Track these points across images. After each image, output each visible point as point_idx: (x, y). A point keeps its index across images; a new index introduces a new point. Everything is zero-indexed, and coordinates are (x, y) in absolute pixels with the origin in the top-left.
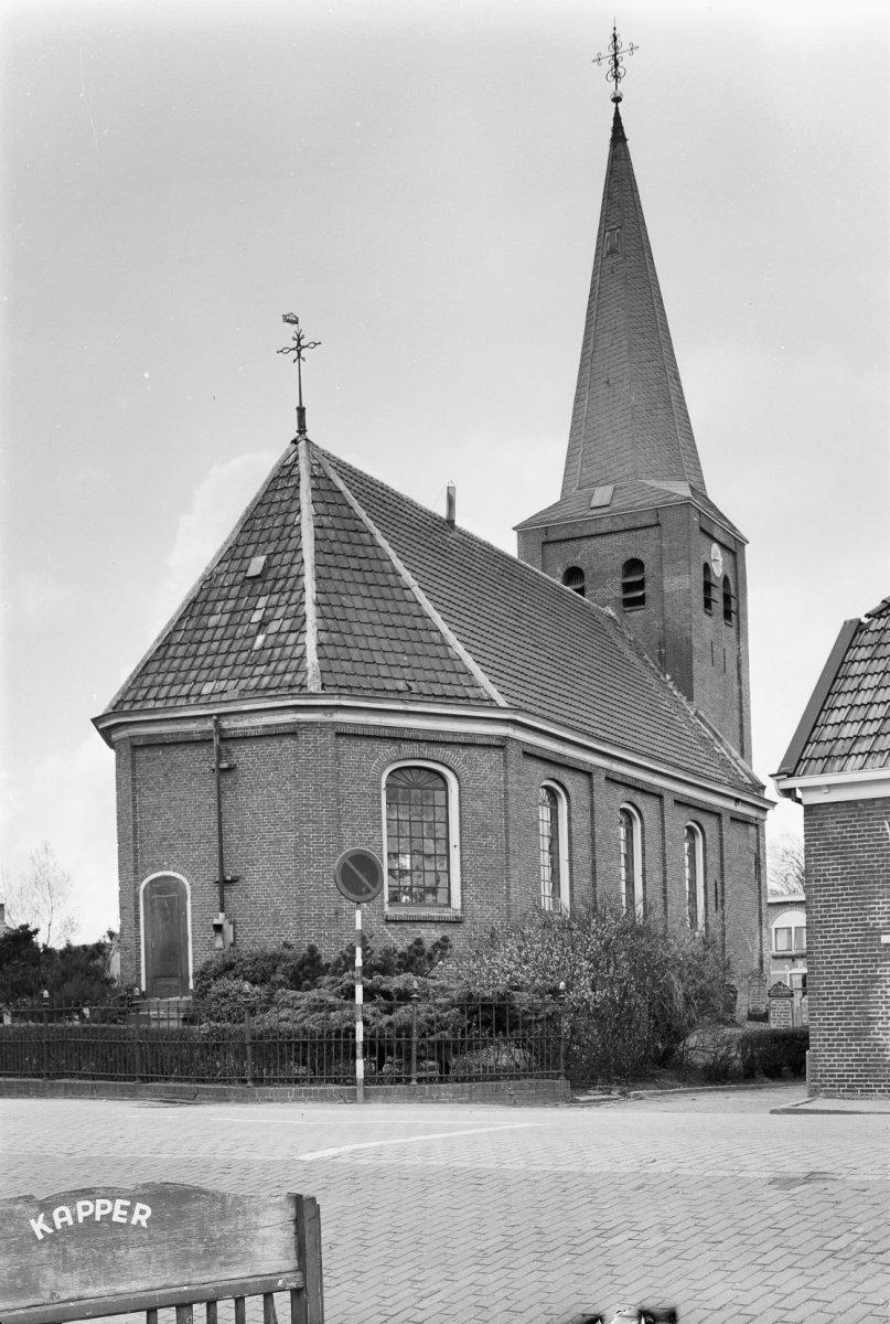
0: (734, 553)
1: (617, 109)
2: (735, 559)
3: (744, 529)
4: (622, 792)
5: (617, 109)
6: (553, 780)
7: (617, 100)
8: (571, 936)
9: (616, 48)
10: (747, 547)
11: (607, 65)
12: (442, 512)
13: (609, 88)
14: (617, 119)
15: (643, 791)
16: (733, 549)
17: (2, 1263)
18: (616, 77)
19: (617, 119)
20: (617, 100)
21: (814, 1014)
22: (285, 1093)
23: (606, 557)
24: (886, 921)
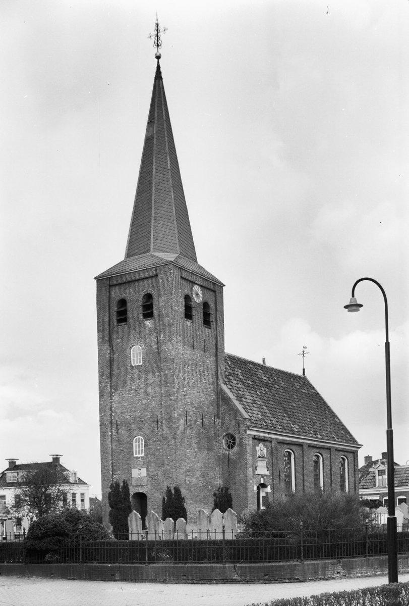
0: (214, 291)
1: (158, 62)
2: (216, 295)
3: (221, 279)
4: (315, 450)
5: (158, 62)
6: (344, 455)
7: (158, 57)
8: (375, 504)
9: (157, 30)
10: (224, 288)
11: (154, 38)
12: (301, 374)
13: (154, 51)
14: (158, 67)
15: (293, 444)
16: (213, 288)
17: (344, 605)
18: (158, 45)
19: (158, 67)
20: (158, 57)
21: (73, 551)
22: (325, 568)
23: (134, 297)
24: (397, 476)
